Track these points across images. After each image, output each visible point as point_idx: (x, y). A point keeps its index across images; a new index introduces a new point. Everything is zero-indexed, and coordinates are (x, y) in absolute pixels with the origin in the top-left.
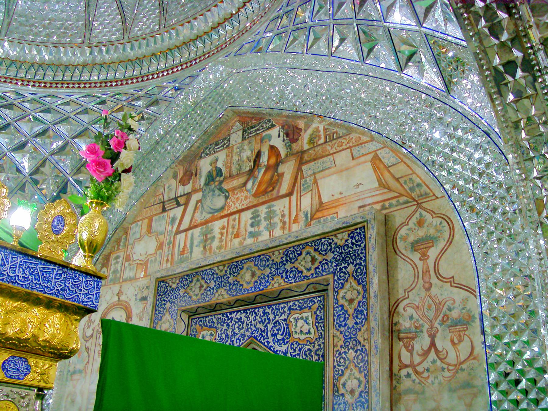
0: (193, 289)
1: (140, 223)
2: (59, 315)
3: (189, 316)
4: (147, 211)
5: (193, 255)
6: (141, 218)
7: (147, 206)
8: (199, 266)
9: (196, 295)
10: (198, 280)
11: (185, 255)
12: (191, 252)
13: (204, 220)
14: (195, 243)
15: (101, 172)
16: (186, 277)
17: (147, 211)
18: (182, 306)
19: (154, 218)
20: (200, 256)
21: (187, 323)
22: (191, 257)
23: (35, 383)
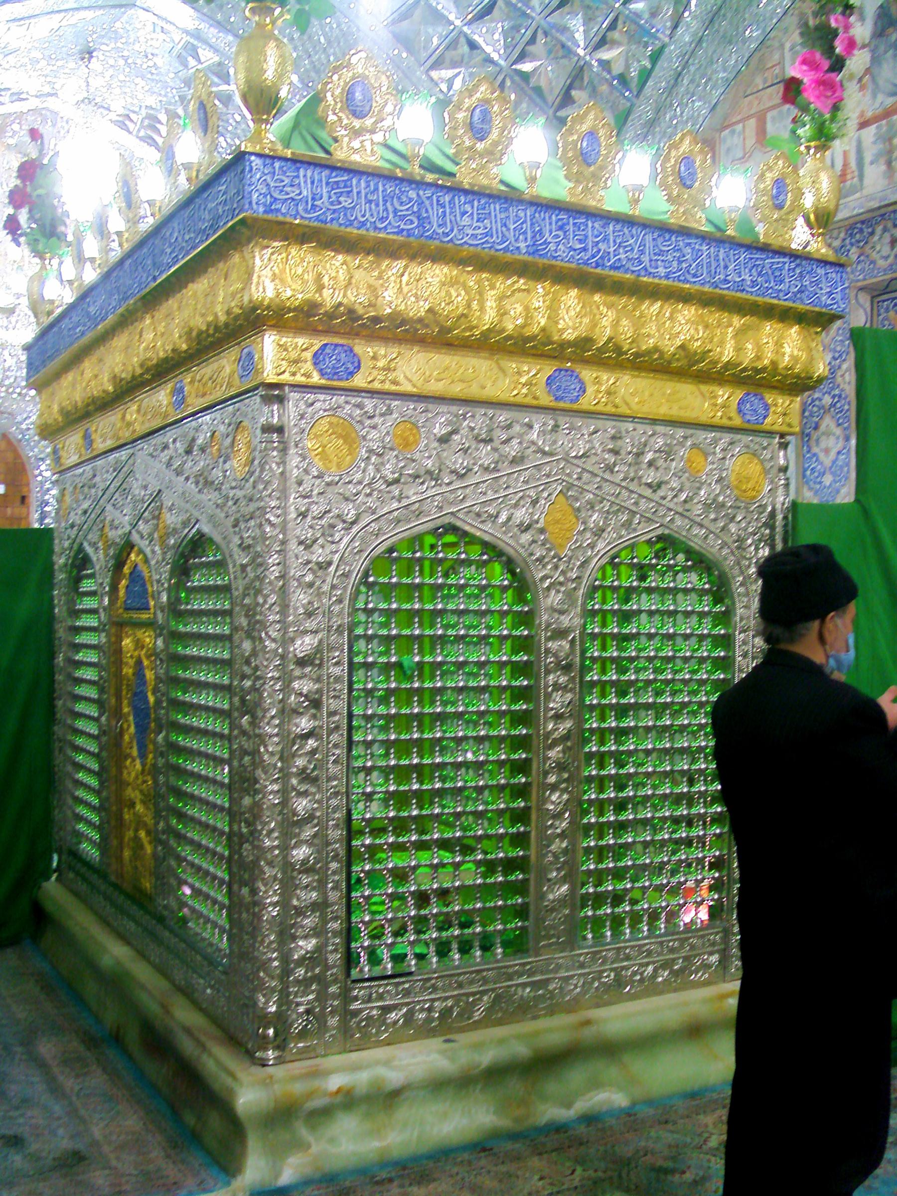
0: (878, 248)
1: (739, 127)
2: (796, 328)
3: (873, 297)
4: (750, 103)
5: (866, 181)
6: (739, 118)
7: (748, 92)
8: (886, 202)
9: (886, 258)
10: (885, 230)
11: (849, 183)
12: (861, 177)
13: (880, 110)
14: (868, 157)
15: (827, 97)
16: (859, 225)
17: (750, 103)
18: (858, 281)
19: (769, 115)
20: (882, 183)
21: (869, 310)
22: (862, 185)
23: (776, 428)
